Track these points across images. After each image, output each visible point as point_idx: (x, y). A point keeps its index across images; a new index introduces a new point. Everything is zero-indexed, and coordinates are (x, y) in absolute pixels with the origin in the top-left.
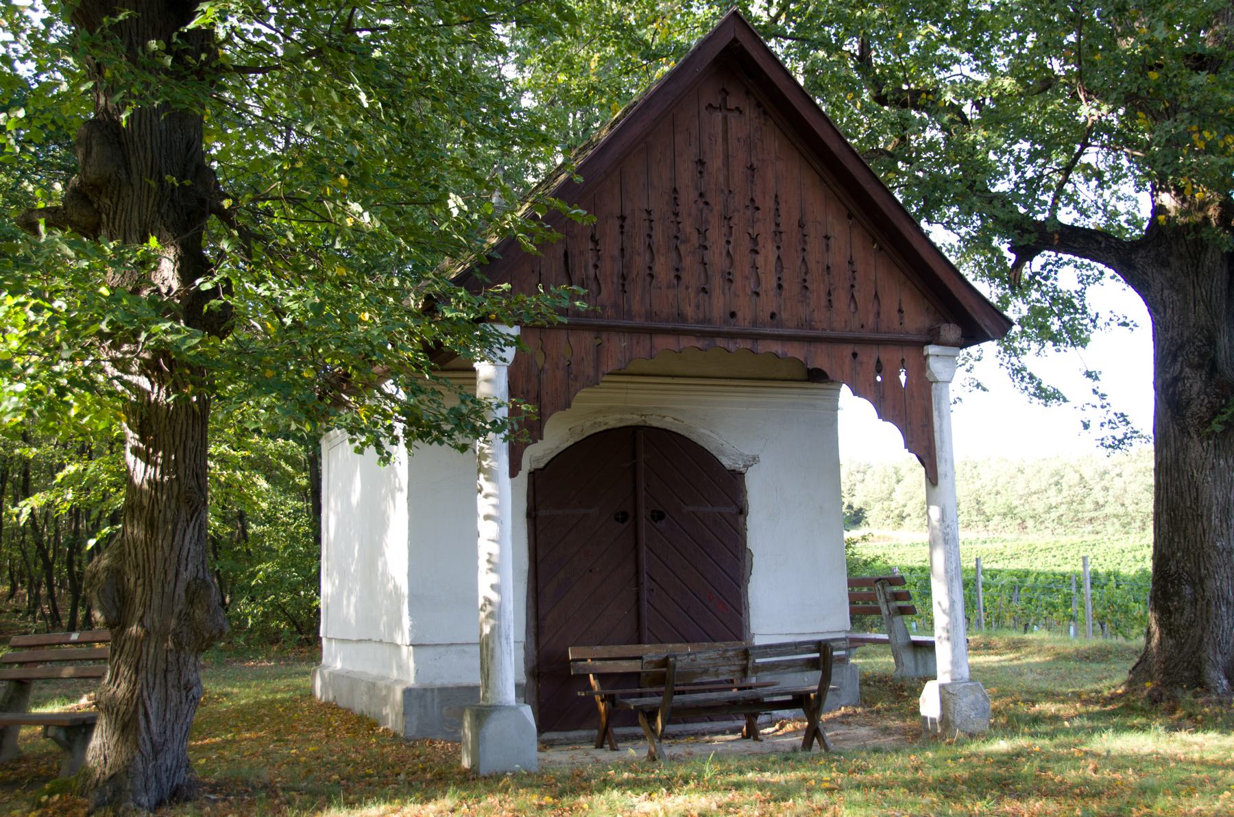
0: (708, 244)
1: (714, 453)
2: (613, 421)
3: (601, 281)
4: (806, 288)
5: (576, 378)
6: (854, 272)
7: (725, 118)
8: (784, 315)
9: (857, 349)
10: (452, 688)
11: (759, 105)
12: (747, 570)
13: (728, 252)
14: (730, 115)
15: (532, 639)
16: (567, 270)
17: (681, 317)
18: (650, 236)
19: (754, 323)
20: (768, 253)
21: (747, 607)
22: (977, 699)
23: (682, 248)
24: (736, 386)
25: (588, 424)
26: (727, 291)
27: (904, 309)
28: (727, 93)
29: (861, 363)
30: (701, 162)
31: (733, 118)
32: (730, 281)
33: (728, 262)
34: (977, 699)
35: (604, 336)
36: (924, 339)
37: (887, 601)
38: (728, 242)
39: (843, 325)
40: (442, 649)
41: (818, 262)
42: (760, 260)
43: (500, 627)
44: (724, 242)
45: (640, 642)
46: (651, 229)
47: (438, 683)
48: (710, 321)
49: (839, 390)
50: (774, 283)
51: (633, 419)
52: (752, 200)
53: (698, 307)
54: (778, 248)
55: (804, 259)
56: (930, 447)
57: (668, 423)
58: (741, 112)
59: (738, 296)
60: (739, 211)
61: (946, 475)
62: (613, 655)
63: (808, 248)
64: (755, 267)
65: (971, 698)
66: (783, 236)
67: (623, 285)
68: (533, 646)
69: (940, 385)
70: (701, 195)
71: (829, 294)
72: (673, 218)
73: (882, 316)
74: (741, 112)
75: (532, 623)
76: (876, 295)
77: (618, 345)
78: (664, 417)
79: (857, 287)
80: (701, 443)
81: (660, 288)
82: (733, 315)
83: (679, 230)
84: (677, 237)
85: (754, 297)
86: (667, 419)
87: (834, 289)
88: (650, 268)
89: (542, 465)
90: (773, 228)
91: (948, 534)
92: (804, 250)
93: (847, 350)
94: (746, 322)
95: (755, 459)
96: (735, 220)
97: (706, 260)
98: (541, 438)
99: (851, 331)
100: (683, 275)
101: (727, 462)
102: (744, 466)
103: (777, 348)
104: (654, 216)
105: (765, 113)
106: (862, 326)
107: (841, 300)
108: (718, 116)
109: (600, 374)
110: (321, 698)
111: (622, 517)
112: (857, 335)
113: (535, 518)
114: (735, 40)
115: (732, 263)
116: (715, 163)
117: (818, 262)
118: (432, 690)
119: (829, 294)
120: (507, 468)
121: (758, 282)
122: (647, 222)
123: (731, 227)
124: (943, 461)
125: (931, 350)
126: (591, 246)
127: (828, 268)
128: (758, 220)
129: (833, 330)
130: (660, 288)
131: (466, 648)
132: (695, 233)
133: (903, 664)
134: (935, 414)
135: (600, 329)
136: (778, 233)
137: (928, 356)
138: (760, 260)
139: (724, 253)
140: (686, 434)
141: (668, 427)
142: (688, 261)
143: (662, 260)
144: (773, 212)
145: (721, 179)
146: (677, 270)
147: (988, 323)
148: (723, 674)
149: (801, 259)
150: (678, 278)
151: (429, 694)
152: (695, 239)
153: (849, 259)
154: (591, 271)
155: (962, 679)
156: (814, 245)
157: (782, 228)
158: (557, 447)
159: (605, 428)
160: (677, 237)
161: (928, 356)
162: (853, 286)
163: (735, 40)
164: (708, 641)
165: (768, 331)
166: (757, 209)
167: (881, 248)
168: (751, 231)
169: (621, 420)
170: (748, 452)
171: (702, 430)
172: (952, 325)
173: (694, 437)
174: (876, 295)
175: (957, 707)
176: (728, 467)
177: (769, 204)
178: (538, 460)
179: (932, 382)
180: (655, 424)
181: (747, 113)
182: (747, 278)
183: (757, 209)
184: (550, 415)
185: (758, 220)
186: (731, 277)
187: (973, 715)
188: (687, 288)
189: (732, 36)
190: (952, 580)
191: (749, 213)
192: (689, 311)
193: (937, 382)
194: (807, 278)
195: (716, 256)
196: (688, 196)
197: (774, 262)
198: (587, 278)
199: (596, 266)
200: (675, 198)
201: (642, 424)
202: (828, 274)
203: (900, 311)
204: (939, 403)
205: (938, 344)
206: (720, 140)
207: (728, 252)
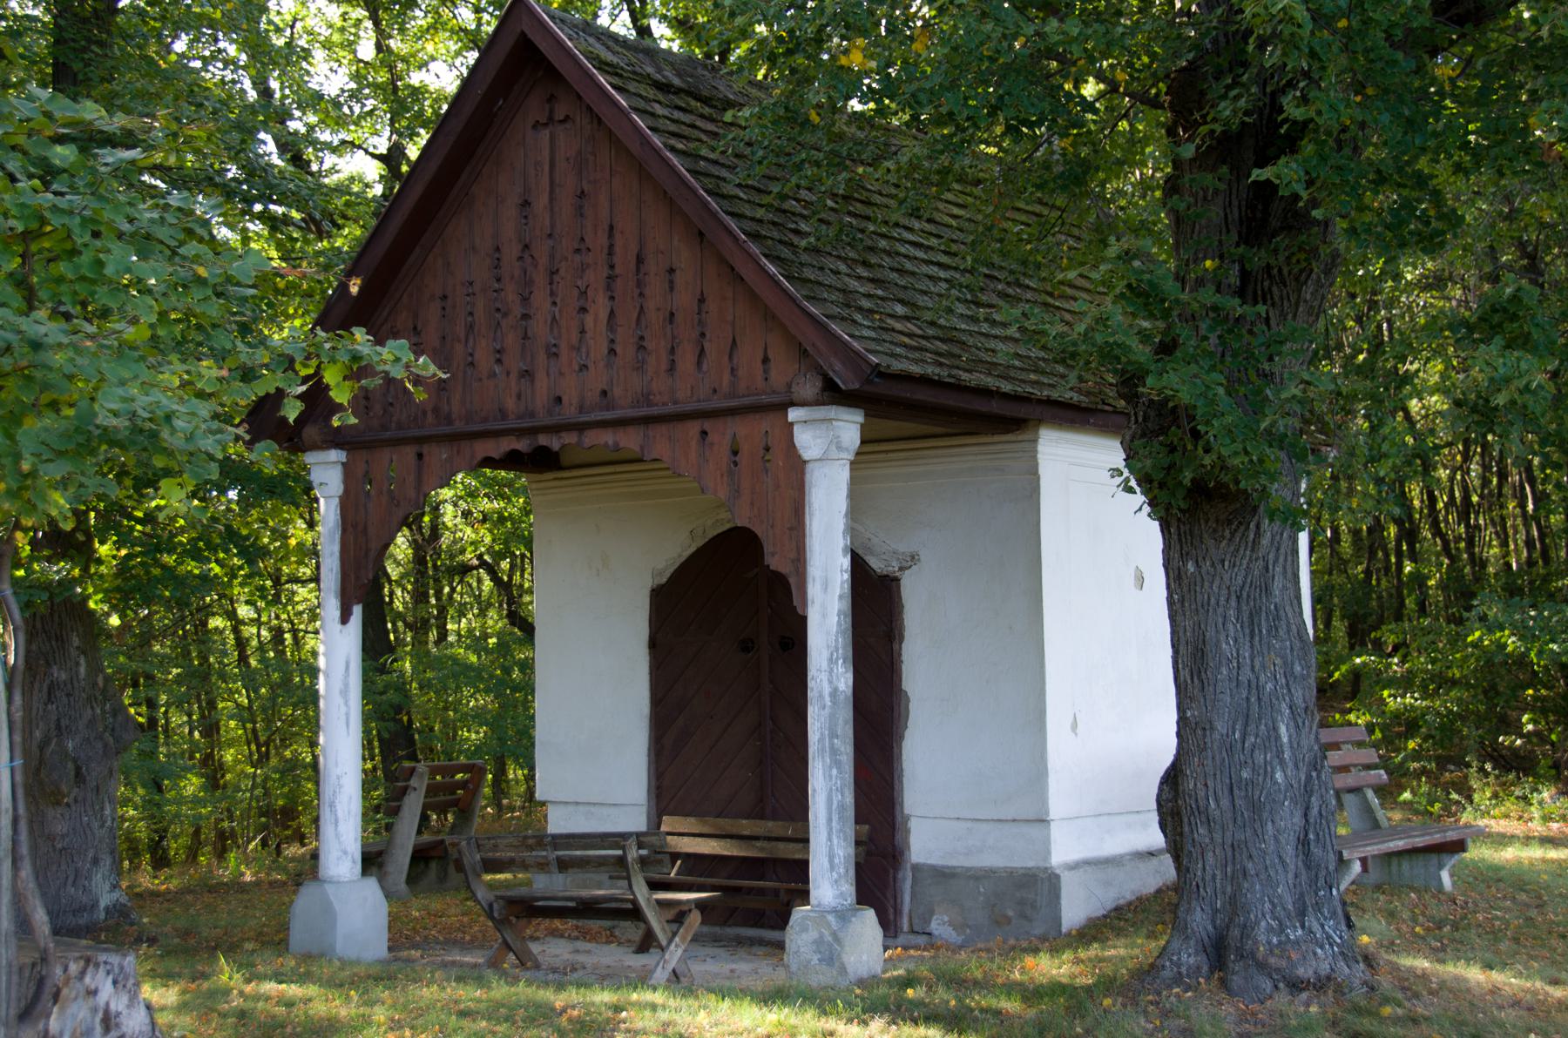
8: (617, 391)
9: (707, 425)
17: (503, 414)
19: (581, 409)
20: (600, 307)
21: (901, 776)
22: (822, 936)
24: (887, 452)
25: (709, 522)
27: (770, 356)
34: (822, 936)
38: (554, 303)
40: (571, 808)
41: (659, 309)
42: (589, 320)
48: (532, 415)
49: (1035, 441)
53: (519, 397)
54: (612, 298)
56: (799, 560)
62: (734, 831)
63: (647, 292)
66: (619, 280)
71: (672, 351)
82: (559, 400)
89: (664, 580)
90: (606, 272)
93: (693, 428)
94: (573, 408)
95: (914, 558)
106: (715, 391)
107: (686, 362)
110: (1400, 865)
116: (541, 202)
117: (659, 309)
119: (672, 351)
125: (794, 414)
127: (672, 314)
128: (588, 266)
129: (675, 403)
130: (480, 380)
131: (593, 809)
135: (420, 440)
137: (792, 424)
147: (838, 366)
156: (655, 285)
157: (618, 270)
158: (680, 556)
161: (792, 424)
162: (703, 335)
165: (593, 417)
168: (579, 283)
170: (903, 548)
177: (603, 240)
178: (660, 574)
185: (588, 266)
187: (815, 961)
192: (510, 404)
195: (539, 327)
196: (511, 252)
197: (605, 322)
203: (766, 360)
206: (547, 168)
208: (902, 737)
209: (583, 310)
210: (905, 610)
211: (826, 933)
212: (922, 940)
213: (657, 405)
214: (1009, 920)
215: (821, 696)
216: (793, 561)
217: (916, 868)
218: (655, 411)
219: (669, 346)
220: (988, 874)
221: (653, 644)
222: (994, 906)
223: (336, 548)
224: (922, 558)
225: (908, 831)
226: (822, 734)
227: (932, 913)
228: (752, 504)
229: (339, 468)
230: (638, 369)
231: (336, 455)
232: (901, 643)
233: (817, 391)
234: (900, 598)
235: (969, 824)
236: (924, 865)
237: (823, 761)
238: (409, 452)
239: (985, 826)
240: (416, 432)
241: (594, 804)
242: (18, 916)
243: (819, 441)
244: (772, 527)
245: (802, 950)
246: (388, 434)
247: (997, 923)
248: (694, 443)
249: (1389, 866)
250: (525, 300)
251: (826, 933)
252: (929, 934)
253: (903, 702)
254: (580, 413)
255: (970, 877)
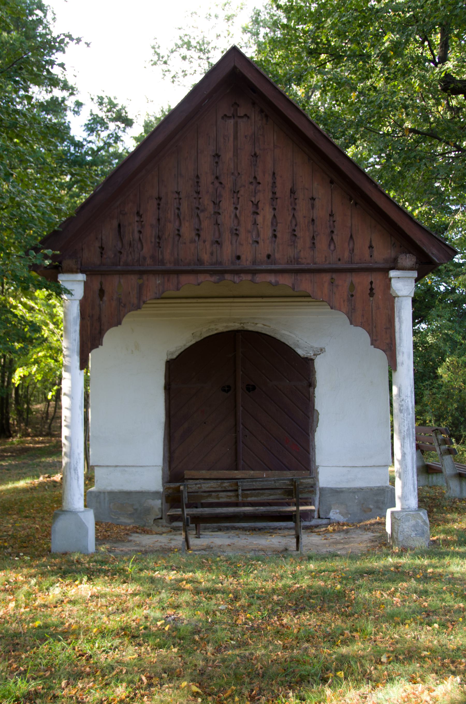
0: (220, 211)
1: (292, 346)
2: (221, 328)
3: (143, 241)
4: (295, 235)
5: (125, 305)
6: (334, 221)
7: (236, 124)
8: (277, 256)
9: (334, 276)
10: (116, 492)
11: (262, 111)
12: (315, 424)
13: (236, 215)
14: (240, 120)
15: (167, 465)
16: (121, 238)
17: (200, 262)
18: (178, 209)
19: (254, 263)
21: (314, 449)
22: (417, 523)
23: (201, 215)
25: (205, 330)
26: (234, 241)
27: (374, 245)
28: (238, 106)
29: (337, 286)
30: (217, 156)
31: (242, 123)
32: (237, 235)
33: (236, 222)
34: (417, 523)
35: (145, 277)
36: (387, 266)
37: (439, 445)
38: (236, 208)
39: (324, 260)
41: (305, 217)
43: (70, 463)
44: (232, 208)
45: (237, 469)
46: (180, 204)
47: (109, 489)
48: (221, 263)
50: (270, 234)
51: (236, 326)
52: (255, 178)
53: (212, 254)
54: (274, 209)
55: (294, 215)
56: (392, 344)
57: (259, 327)
58: (248, 117)
59: (242, 245)
60: (244, 186)
61: (402, 364)
62: (213, 477)
63: (297, 207)
64: (255, 223)
65: (413, 522)
66: (279, 201)
67: (159, 243)
68: (167, 468)
69: (400, 299)
70: (217, 178)
71: (313, 238)
72: (195, 195)
73: (355, 251)
74: (248, 117)
75: (167, 455)
76: (351, 237)
77: (156, 281)
78: (257, 324)
79: (335, 232)
80: (283, 340)
81: (185, 243)
82: (238, 258)
83: (199, 204)
84: (198, 208)
85: (255, 244)
86: (259, 325)
87: (317, 235)
88: (178, 230)
89: (174, 357)
90: (270, 195)
91: (402, 406)
92: (294, 209)
93: (326, 277)
94: (248, 263)
95: (322, 350)
96: (242, 192)
97: (219, 222)
98: (102, 345)
99: (330, 264)
100: (202, 233)
101: (301, 352)
102: (314, 355)
103: (272, 278)
104: (182, 196)
105: (267, 116)
106: (339, 260)
108: (231, 122)
109: (142, 302)
110: (432, 478)
111: (227, 389)
112: (334, 266)
113: (169, 389)
114: (235, 68)
115: (239, 224)
116: (227, 156)
117: (305, 217)
118: (104, 493)
119: (313, 238)
120: (78, 364)
121: (258, 235)
122: (178, 200)
123: (239, 198)
124: (401, 354)
125: (392, 274)
126: (137, 219)
128: (259, 191)
130: (185, 243)
131: (126, 469)
132: (212, 204)
133: (450, 488)
134: (397, 320)
135: (141, 273)
136: (274, 199)
138: (260, 219)
139: (233, 216)
140: (272, 335)
141: (259, 330)
142: (206, 224)
143: (187, 224)
144: (270, 185)
145: (232, 166)
146: (198, 230)
147: (435, 251)
148: (222, 497)
149: (291, 215)
150: (199, 235)
151: (102, 495)
152: (211, 208)
153: (330, 212)
154: (137, 235)
155: (409, 508)
157: (278, 195)
158: (185, 345)
159: (215, 332)
160: (198, 208)
162: (332, 232)
163: (235, 68)
164: (304, 470)
165: (263, 267)
166: (259, 183)
167: (356, 204)
168: (253, 199)
169: (227, 327)
170: (316, 345)
171: (283, 332)
172: (408, 255)
173: (278, 337)
174: (351, 237)
175: (400, 529)
176: (302, 355)
177: (268, 179)
178: (172, 353)
179: (395, 297)
180: (250, 328)
181: (253, 117)
182: (249, 232)
183: (259, 183)
184: (107, 330)
185: (259, 191)
186: (237, 232)
187: (413, 534)
188: (204, 242)
189: (233, 65)
190: (404, 438)
191: (252, 187)
192: (206, 257)
193: (398, 297)
194: (296, 229)
197: (270, 220)
198: (133, 240)
199: (140, 232)
200: (198, 182)
201: (242, 329)
202: (313, 224)
203: (371, 247)
204: (399, 312)
205: (399, 269)
206: (232, 139)
207: (236, 215)
208: (315, 431)
209: (256, 213)
210: (317, 374)
211: (420, 521)
212: (325, 521)
213: (303, 264)
214: (371, 510)
215: (408, 408)
216: (388, 344)
217: (322, 489)
218: (354, 266)
219: (312, 236)
220: (360, 490)
221: (168, 388)
222: (363, 504)
223: (78, 328)
224: (326, 350)
225: (318, 473)
226: (409, 427)
227: (330, 509)
228: (363, 316)
229: (82, 284)
230: (291, 245)
231: (81, 277)
232: (314, 388)
233: (413, 263)
234: (314, 368)
235: (349, 469)
236: (326, 488)
237: (410, 440)
238: (133, 280)
239: (357, 469)
240: (137, 268)
241: (130, 466)
242: (56, 554)
243: (407, 287)
244: (375, 327)
245: (405, 530)
246: (119, 268)
247: (365, 511)
248: (326, 285)
249: (428, 478)
250: (216, 204)
251: (420, 521)
252: (329, 518)
253: (315, 416)
254: (253, 264)
255: (351, 492)
